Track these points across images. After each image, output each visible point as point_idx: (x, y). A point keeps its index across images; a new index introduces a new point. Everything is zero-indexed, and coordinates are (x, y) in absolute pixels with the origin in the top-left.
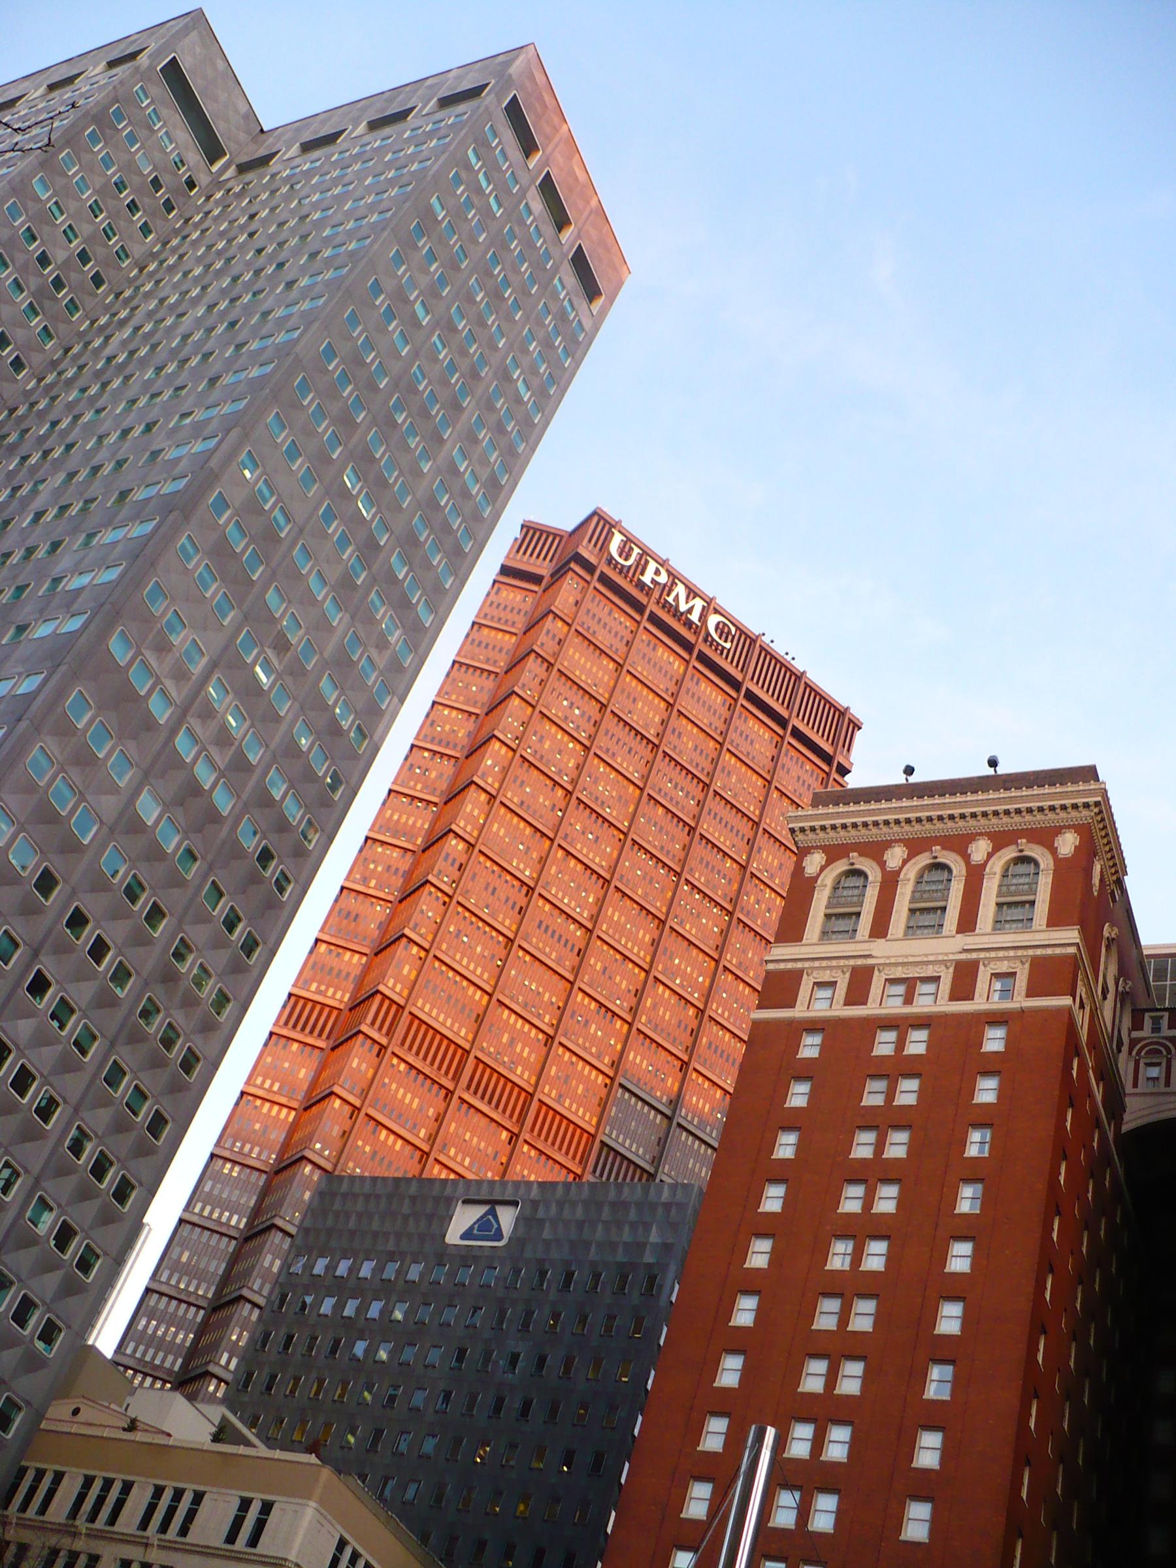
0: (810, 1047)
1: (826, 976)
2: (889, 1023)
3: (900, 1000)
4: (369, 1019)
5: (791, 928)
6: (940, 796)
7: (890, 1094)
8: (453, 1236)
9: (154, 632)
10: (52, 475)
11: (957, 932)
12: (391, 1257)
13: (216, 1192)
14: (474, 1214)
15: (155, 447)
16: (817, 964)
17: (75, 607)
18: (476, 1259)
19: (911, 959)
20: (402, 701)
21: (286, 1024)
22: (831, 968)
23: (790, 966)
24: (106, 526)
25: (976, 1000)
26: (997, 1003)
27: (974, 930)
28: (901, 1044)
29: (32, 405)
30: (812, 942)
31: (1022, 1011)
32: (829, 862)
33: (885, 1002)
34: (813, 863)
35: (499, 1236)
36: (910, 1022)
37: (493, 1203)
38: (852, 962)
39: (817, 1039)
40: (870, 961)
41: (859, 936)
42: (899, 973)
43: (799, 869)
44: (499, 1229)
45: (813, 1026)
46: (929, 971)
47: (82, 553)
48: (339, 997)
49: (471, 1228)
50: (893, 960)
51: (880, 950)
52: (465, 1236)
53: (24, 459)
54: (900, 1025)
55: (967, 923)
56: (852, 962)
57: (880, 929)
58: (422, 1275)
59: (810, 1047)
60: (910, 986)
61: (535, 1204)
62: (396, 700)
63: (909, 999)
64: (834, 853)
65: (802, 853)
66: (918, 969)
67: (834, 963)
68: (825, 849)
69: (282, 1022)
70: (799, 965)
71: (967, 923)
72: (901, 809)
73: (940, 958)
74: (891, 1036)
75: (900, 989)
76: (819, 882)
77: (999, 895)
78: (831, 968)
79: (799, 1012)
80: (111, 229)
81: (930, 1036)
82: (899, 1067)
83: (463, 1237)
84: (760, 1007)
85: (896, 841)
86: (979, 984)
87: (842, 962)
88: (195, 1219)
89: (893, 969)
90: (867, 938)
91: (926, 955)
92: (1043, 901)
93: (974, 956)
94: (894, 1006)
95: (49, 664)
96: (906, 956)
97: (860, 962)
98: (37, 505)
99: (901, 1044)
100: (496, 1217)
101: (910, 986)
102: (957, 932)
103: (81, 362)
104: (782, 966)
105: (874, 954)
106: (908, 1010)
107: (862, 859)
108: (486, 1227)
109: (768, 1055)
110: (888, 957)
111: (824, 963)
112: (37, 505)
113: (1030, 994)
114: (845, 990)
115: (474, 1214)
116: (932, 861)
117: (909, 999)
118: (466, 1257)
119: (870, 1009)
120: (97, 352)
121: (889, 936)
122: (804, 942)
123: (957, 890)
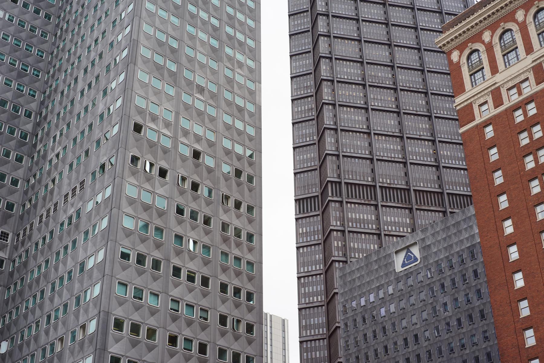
0: (489, 132)
1: (482, 101)
2: (516, 108)
3: (517, 95)
4: (330, 194)
5: (459, 88)
6: (472, 15)
7: (531, 136)
8: (399, 268)
9: (148, 114)
10: (79, 73)
11: (527, 55)
12: (379, 288)
13: (311, 291)
14: (401, 257)
15: (110, 42)
16: (476, 97)
17: (113, 123)
18: (411, 273)
19: (513, 76)
20: (260, 82)
21: (300, 212)
22: (482, 96)
23: (466, 103)
24: (108, 84)
25: (505, 104)
26: (486, 116)
27: (533, 51)
28: (525, 113)
29: (58, 47)
30: (470, 91)
31: (536, 93)
32: (461, 53)
33: (511, 98)
34: (455, 56)
35: (416, 259)
36: (524, 102)
37: (408, 248)
38: (490, 89)
39: (532, 105)
40: (497, 85)
41: (486, 77)
42: (510, 84)
43: (450, 62)
44: (415, 256)
45: (486, 124)
46: (523, 77)
47: (105, 99)
48: (316, 191)
49: (404, 261)
50: (506, 80)
51: (499, 78)
52: (403, 266)
53: (66, 71)
54: (522, 105)
55: (529, 49)
56: (490, 89)
57: (494, 70)
58: (393, 289)
59: (489, 132)
60: (518, 86)
61: (423, 240)
62: (257, 84)
63: (520, 93)
64: (461, 48)
65: (449, 54)
66: (518, 79)
67: (483, 93)
68: (457, 48)
69: (298, 213)
70: (469, 101)
71: (529, 49)
72: (480, 15)
73: (525, 69)
74: (520, 112)
75: (515, 90)
76: (461, 63)
77: (537, 30)
78: (482, 96)
79: (478, 120)
80: (8, 85)
81: (536, 104)
82: (529, 124)
83: (402, 267)
84: (462, 126)
85: (484, 29)
86: (475, 113)
87: (486, 92)
88: (305, 306)
89: (508, 84)
90: (526, 56)
91: (518, 71)
92: (521, 45)
93: (538, 61)
94: (515, 98)
95: (114, 151)
96: (510, 76)
97: (493, 88)
98: (79, 88)
99: (525, 113)
100: (411, 252)
101: (518, 86)
102: (527, 55)
103: (66, 20)
104: (462, 105)
105: (497, 81)
106: (521, 98)
107: (474, 45)
108: (409, 258)
109: (473, 144)
110: (503, 80)
111: (479, 96)
112: (79, 88)
113: (538, 83)
114: (534, 79)
115: (401, 257)
116: (503, 30)
117: (520, 93)
118: (408, 275)
119: (507, 104)
120: (70, 12)
121: (500, 71)
122: (467, 91)
123: (518, 37)
